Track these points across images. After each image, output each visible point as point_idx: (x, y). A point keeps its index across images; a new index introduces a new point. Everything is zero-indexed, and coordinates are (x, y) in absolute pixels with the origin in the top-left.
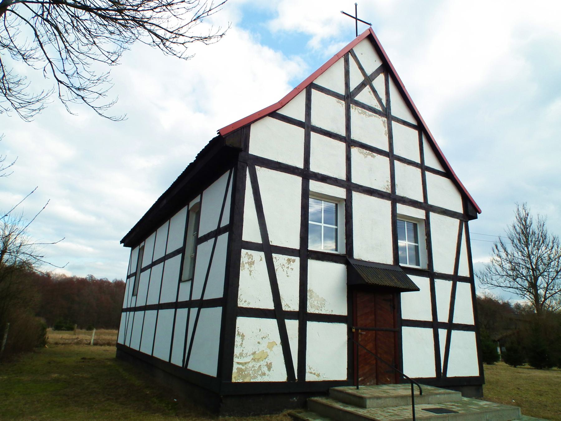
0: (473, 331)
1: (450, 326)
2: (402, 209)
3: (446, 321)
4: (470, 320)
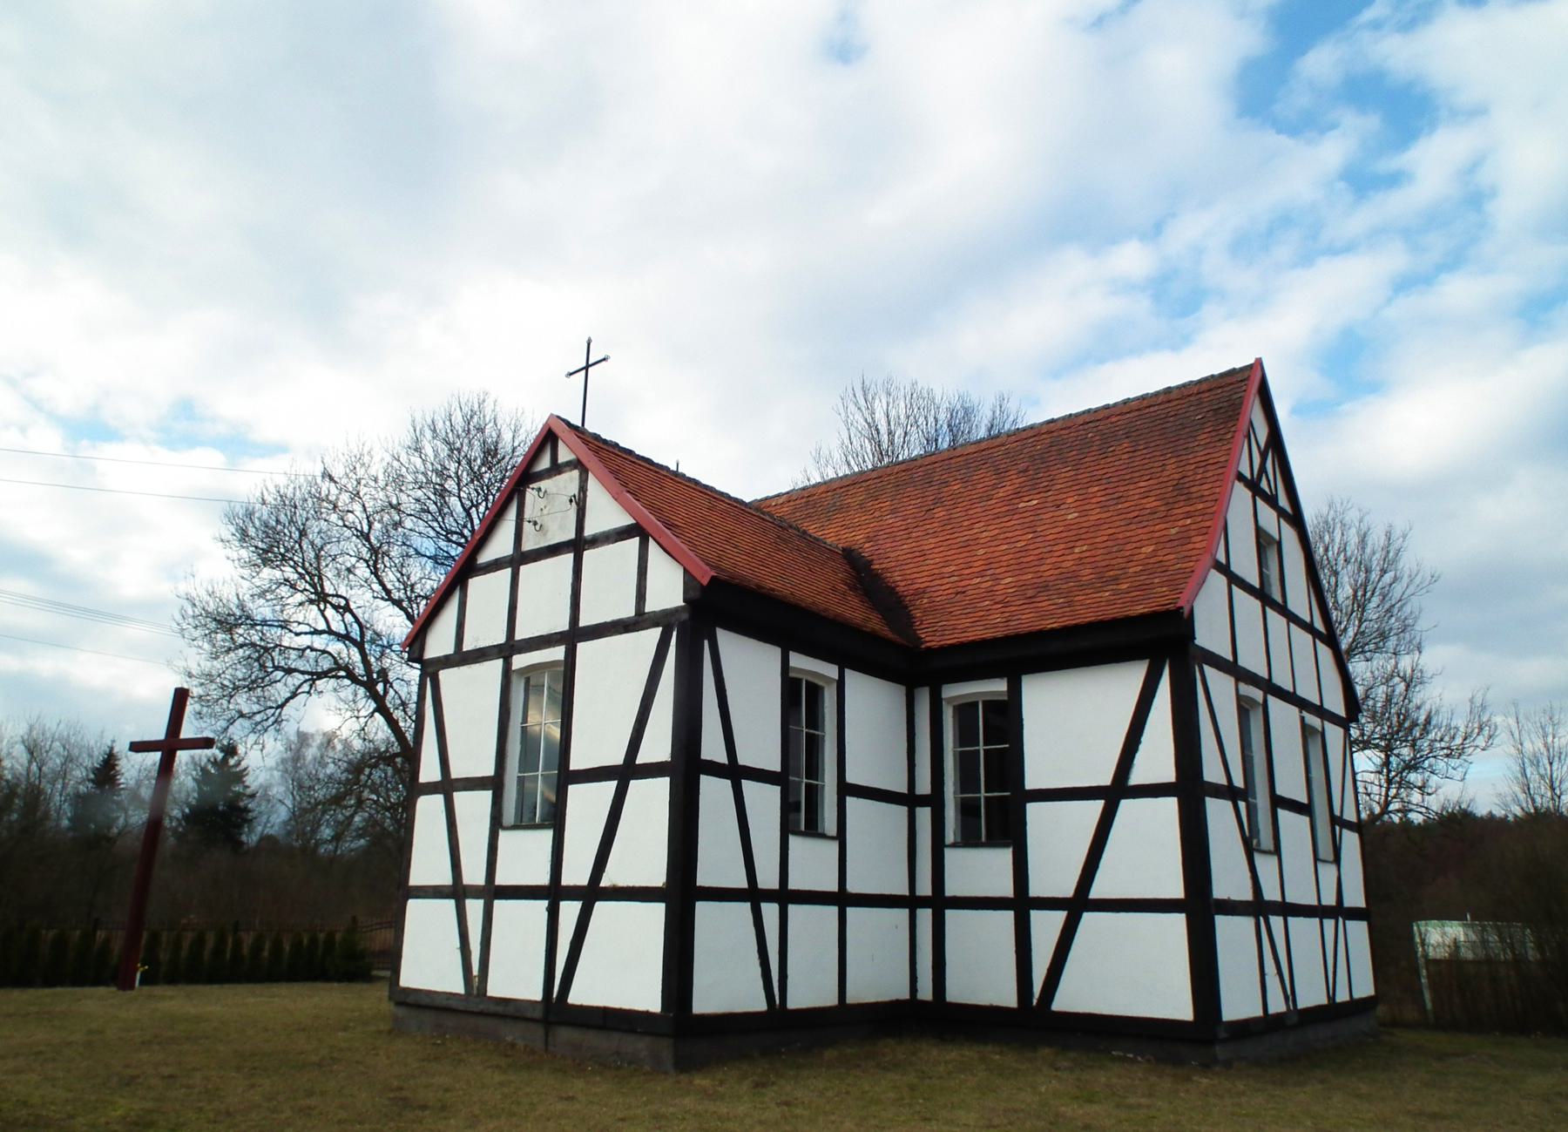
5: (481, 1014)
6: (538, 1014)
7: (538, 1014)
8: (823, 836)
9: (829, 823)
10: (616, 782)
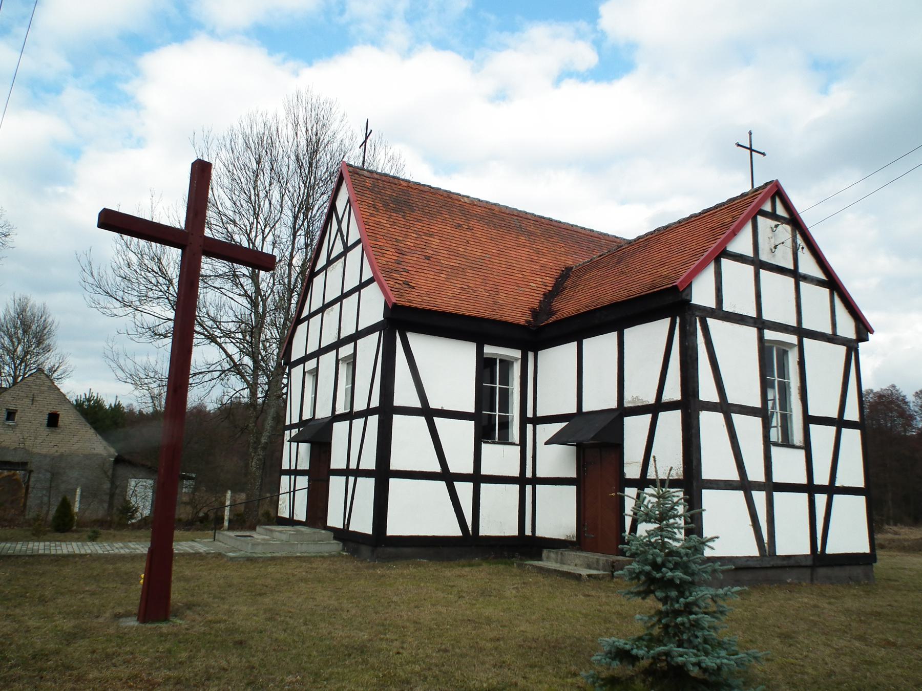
0: (453, 473)
1: (831, 490)
2: (769, 335)
3: (826, 482)
4: (859, 481)
5: (773, 567)
6: (809, 563)
7: (809, 563)
8: (794, 447)
9: (797, 437)
10: (434, 418)
